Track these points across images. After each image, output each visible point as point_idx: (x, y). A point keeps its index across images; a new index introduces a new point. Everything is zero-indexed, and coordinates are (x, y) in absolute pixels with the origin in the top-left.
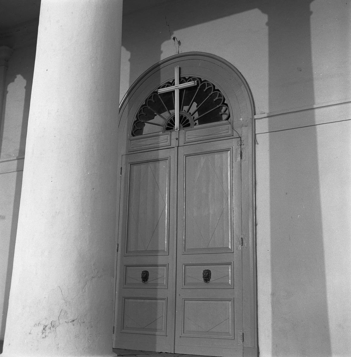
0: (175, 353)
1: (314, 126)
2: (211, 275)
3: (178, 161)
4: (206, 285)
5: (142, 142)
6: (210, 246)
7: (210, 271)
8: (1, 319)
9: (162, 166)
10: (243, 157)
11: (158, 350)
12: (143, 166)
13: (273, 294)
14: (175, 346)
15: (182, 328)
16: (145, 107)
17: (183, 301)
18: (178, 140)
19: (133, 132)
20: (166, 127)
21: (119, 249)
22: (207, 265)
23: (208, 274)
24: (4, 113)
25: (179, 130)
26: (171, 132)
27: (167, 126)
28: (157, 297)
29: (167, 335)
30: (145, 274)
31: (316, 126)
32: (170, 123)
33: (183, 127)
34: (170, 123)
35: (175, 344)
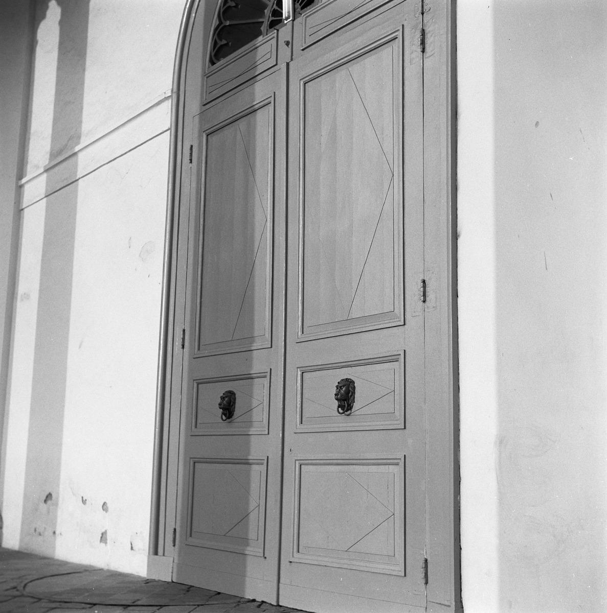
0: (280, 604)
1: (247, 436)
2: (354, 393)
3: (171, 420)
4: (342, 422)
5: (232, 64)
6: (355, 315)
7: (354, 382)
8: (1, 357)
9: (262, 119)
10: (427, 46)
11: (249, 596)
12: (228, 132)
13: (501, 442)
14: (280, 585)
15: (293, 541)
16: (222, 26)
17: (298, 466)
18: (290, 46)
19: (213, 54)
20: (270, 20)
21: (187, 344)
22: (348, 366)
23: (347, 392)
24: (33, 82)
25: (293, 20)
26: (278, 30)
27: (271, 19)
28: (250, 457)
29: (265, 556)
30: (226, 399)
31: (249, 436)
32: (273, 18)
33: (302, 8)
34: (273, 18)
35: (281, 581)
